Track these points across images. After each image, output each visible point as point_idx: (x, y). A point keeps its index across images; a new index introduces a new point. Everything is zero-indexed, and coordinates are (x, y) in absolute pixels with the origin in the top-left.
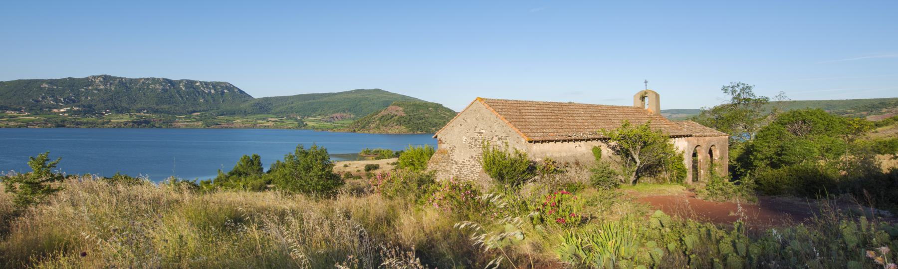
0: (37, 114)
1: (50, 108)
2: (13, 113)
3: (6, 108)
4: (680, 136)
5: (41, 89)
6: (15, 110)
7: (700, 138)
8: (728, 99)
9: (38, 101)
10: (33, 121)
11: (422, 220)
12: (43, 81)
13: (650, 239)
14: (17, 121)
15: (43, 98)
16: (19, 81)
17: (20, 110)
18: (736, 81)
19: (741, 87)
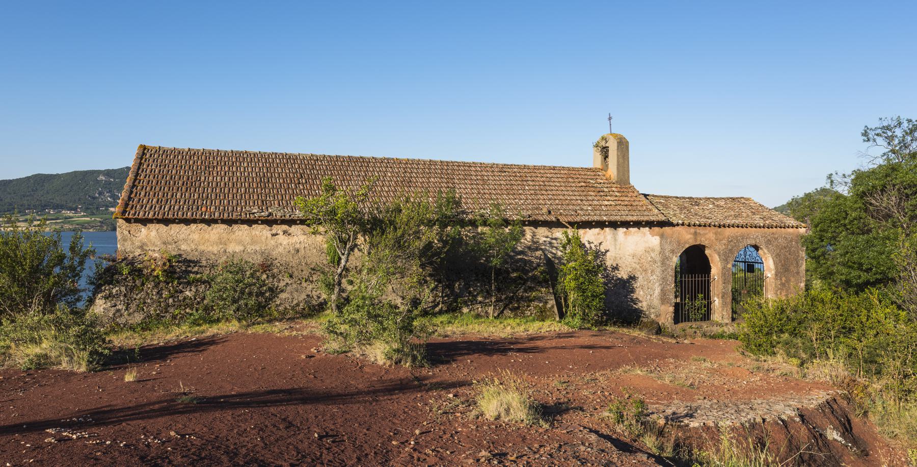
0: (93, 214)
1: (107, 206)
2: (69, 213)
3: (62, 207)
4: (638, 224)
5: (98, 182)
6: (71, 209)
7: (700, 230)
8: (874, 156)
9: (94, 198)
10: (88, 223)
11: (914, 254)
12: (99, 172)
13: (686, 416)
14: (71, 223)
15: (100, 194)
16: (75, 172)
17: (75, 209)
18: (889, 115)
19: (905, 125)
